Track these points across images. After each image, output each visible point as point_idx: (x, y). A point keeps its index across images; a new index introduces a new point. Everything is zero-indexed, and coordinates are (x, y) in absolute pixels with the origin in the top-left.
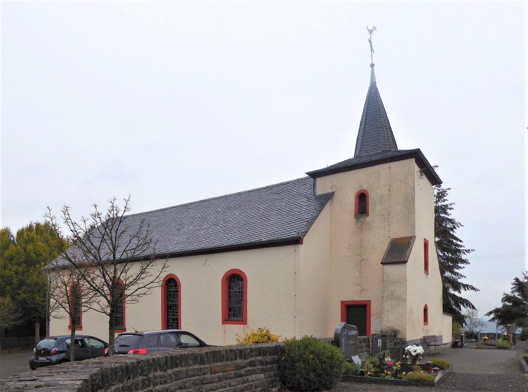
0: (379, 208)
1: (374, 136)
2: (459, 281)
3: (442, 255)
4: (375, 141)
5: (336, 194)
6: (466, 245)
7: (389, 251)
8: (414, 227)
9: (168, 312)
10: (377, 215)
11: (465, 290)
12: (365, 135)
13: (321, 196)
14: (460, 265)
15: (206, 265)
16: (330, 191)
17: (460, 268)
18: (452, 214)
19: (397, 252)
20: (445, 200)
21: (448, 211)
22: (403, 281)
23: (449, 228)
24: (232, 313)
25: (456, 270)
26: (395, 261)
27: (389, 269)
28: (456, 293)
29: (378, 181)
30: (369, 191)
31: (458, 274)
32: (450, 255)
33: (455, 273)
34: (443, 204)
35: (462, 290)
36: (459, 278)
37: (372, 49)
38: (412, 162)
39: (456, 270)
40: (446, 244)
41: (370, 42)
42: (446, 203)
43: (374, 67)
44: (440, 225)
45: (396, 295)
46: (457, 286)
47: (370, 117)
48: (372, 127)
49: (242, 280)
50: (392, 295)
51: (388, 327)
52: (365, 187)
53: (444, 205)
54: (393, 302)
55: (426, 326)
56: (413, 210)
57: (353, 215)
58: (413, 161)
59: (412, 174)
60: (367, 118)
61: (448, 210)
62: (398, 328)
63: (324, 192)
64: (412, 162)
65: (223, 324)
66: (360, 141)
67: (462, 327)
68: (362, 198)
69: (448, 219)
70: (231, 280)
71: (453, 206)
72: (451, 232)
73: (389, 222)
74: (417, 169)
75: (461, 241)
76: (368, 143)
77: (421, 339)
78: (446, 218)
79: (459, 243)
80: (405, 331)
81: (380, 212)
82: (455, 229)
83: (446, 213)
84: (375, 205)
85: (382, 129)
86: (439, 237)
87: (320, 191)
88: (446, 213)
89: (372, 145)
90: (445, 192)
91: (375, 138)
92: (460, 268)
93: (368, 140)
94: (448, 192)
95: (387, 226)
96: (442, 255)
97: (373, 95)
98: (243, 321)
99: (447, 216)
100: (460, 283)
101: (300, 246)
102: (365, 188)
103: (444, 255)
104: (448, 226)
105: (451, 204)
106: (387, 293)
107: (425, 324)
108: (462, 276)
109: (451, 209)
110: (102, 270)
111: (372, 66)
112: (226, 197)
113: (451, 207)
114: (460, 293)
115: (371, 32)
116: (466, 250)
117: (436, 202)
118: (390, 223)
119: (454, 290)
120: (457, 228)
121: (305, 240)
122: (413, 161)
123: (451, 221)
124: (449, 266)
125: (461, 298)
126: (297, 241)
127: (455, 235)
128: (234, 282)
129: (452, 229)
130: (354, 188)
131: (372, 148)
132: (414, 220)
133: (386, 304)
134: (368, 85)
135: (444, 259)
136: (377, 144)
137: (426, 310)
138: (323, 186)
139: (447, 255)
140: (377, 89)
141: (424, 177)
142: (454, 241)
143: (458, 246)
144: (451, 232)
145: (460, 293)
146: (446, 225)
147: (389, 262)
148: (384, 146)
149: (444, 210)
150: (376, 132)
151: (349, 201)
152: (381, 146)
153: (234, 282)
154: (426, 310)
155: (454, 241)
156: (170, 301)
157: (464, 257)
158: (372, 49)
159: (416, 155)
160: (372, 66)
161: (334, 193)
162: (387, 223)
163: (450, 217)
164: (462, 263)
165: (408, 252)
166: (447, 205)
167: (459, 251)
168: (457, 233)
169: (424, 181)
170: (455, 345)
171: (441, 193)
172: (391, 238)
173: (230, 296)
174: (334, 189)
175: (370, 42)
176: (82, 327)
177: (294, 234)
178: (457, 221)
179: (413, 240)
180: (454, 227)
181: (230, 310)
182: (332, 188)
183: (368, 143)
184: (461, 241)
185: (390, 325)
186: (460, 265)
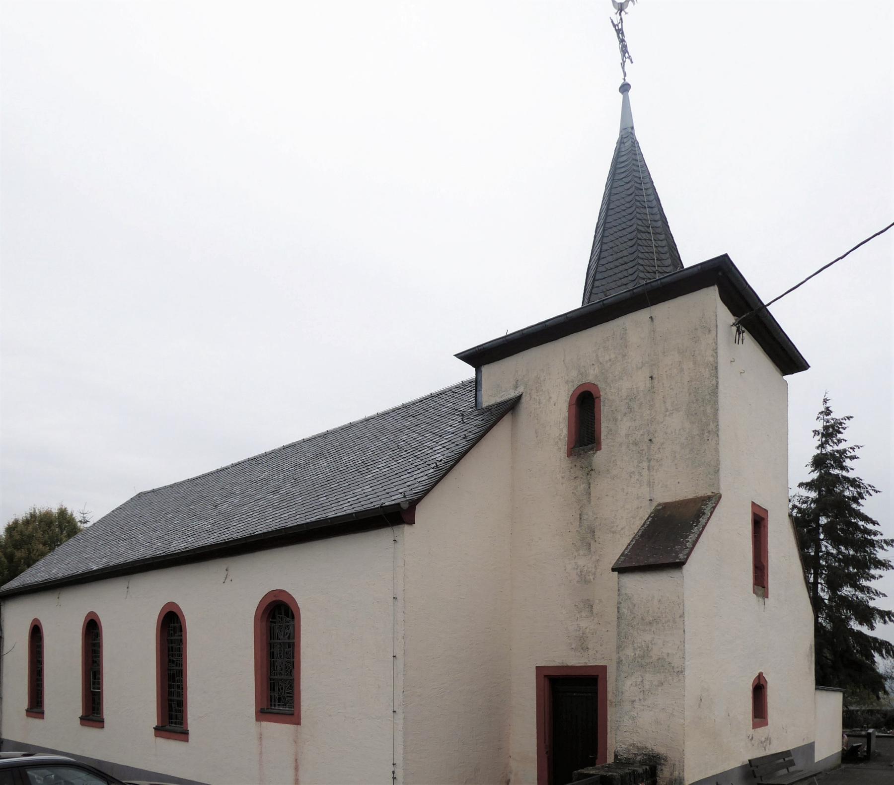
0: (625, 426)
1: (625, 253)
2: (872, 604)
3: (834, 552)
4: (625, 267)
5: (523, 400)
6: (887, 530)
7: (641, 536)
8: (717, 471)
9: (170, 686)
10: (621, 445)
11: (885, 622)
12: (603, 255)
13: (489, 409)
14: (873, 572)
15: (228, 580)
16: (512, 394)
17: (873, 577)
18: (856, 469)
19: (665, 540)
20: (840, 441)
21: (848, 463)
22: (672, 618)
23: (848, 498)
24: (277, 696)
25: (864, 583)
26: (651, 561)
27: (635, 583)
28: (865, 630)
29: (624, 356)
30: (601, 385)
31: (869, 589)
32: (851, 552)
33: (862, 589)
34: (836, 448)
35: (878, 624)
36: (871, 599)
37: (624, 50)
38: (711, 297)
39: (864, 583)
40: (842, 530)
41: (620, 32)
42: (841, 447)
43: (631, 93)
44: (830, 491)
45: (655, 658)
46: (867, 615)
47: (618, 210)
48: (620, 234)
49: (293, 617)
50: (643, 657)
51: (633, 745)
52: (592, 376)
53: (838, 451)
54: (648, 677)
55: (760, 730)
56: (712, 426)
57: (564, 448)
58: (713, 293)
59: (709, 328)
60: (611, 212)
61: (848, 460)
62: (661, 750)
63: (499, 399)
64: (710, 298)
65: (258, 719)
66: (592, 272)
67: (878, 698)
68: (586, 405)
69: (847, 479)
70: (274, 617)
71: (857, 453)
72: (854, 506)
73: (649, 461)
74: (725, 317)
75: (874, 523)
76: (611, 273)
77: (743, 767)
78: (844, 477)
79: (870, 526)
80: (682, 761)
81: (627, 436)
82: (863, 498)
83: (843, 468)
84: (616, 420)
85: (644, 236)
86: (828, 517)
87: (489, 399)
88: (843, 468)
89: (620, 275)
90: (841, 424)
91: (625, 259)
92: (873, 577)
93: (612, 265)
94: (847, 423)
95: (645, 473)
96: (834, 552)
97: (624, 158)
98: (293, 714)
99: (845, 473)
100: (874, 609)
101: (406, 528)
102: (591, 379)
103: (840, 552)
104: (847, 493)
105: (853, 448)
106: (629, 652)
107: (755, 726)
108: (877, 594)
109: (852, 458)
110: (812, 580)
111: (625, 88)
112: (325, 435)
113: (853, 454)
114: (872, 628)
115: (621, 8)
116: (885, 542)
117: (822, 446)
118: (652, 463)
119: (861, 624)
120: (867, 496)
121: (421, 512)
122: (713, 293)
123: (854, 483)
124: (850, 574)
125: (875, 640)
126: (396, 516)
127: (863, 510)
128: (278, 620)
129: (855, 500)
130: (567, 382)
131: (619, 283)
132: (717, 451)
133: (629, 682)
134: (616, 136)
135: (840, 561)
136: (630, 271)
137: (759, 689)
138: (500, 381)
139: (846, 552)
140: (635, 144)
141: (746, 336)
142: (861, 523)
143: (869, 532)
144: (854, 506)
145: (872, 628)
146: (843, 491)
147: (634, 564)
148: (648, 275)
149: (839, 459)
150: (630, 243)
151: (552, 414)
152: (642, 275)
153: (278, 620)
154: (759, 689)
155: (861, 523)
156: (173, 662)
157: (881, 555)
158: (624, 50)
159: (721, 275)
160: (625, 88)
161: (518, 399)
162: (645, 464)
163: (851, 475)
164: (876, 567)
165: (692, 538)
166: (845, 451)
167: (872, 544)
168: (867, 507)
169: (750, 350)
170: (849, 755)
171: (833, 426)
172: (655, 504)
173: (272, 655)
174: (521, 390)
175: (620, 32)
176: (43, 713)
177: (393, 497)
178: (866, 482)
179: (710, 505)
180: (861, 496)
181: (272, 687)
182: (516, 387)
183: (611, 273)
184: (874, 523)
185: (636, 739)
186: (873, 572)
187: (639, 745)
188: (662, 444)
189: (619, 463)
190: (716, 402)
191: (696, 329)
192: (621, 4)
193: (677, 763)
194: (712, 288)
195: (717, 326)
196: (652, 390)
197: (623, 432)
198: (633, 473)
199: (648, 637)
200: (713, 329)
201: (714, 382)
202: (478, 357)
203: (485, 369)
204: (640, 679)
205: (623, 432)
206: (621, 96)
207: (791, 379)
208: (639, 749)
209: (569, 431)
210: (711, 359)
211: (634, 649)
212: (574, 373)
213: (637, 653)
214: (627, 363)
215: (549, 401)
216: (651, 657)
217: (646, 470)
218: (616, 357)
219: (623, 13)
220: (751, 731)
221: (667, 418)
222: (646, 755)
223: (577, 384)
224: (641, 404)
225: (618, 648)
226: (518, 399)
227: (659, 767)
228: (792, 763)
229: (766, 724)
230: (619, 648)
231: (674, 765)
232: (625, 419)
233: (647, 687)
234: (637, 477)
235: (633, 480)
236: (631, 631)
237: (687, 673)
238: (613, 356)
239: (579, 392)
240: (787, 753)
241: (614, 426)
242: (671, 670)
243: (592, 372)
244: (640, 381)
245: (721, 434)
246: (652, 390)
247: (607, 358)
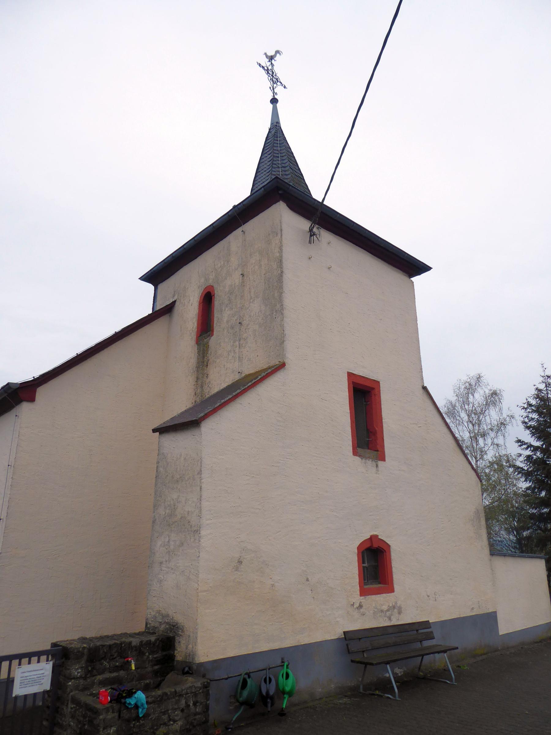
5: (177, 303)
30: (215, 286)
43: (278, 105)
45: (179, 516)
51: (159, 612)
62: (179, 619)
81: (228, 322)
95: (237, 350)
106: (161, 511)
118: (242, 342)
132: (282, 326)
161: (174, 303)
162: (237, 343)
182: (174, 296)
187: (163, 612)
188: (248, 325)
189: (222, 344)
190: (281, 287)
191: (269, 235)
192: (272, 56)
193: (191, 635)
194: (278, 203)
195: (281, 230)
196: (243, 284)
197: (225, 320)
198: (230, 351)
199: (175, 496)
200: (279, 232)
201: (279, 272)
202: (156, 277)
203: (160, 286)
204: (167, 540)
205: (225, 320)
206: (272, 106)
207: (416, 279)
208: (163, 616)
209: (198, 324)
210: (278, 255)
211: (165, 508)
212: (202, 280)
213: (167, 511)
214: (230, 266)
215: (189, 302)
216: (176, 515)
217: (238, 348)
218: (224, 263)
219: (273, 61)
220: (357, 598)
221: (251, 304)
222: (167, 623)
223: (204, 287)
224: (236, 296)
225: (154, 507)
226: (174, 303)
227: (177, 638)
228: (430, 636)
229: (392, 591)
230: (156, 506)
231: (189, 636)
232: (227, 309)
233: (172, 547)
234: (232, 354)
235: (230, 357)
236: (164, 490)
237: (203, 533)
238: (222, 263)
239: (205, 293)
240: (426, 624)
241: (222, 316)
242: (190, 529)
243: (211, 277)
244: (236, 279)
245: (286, 312)
246: (243, 284)
247: (219, 265)
